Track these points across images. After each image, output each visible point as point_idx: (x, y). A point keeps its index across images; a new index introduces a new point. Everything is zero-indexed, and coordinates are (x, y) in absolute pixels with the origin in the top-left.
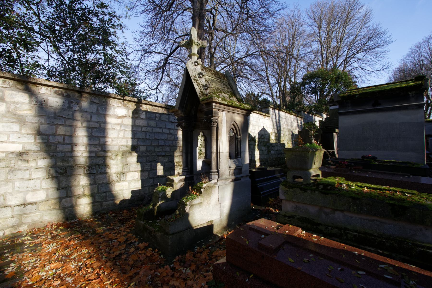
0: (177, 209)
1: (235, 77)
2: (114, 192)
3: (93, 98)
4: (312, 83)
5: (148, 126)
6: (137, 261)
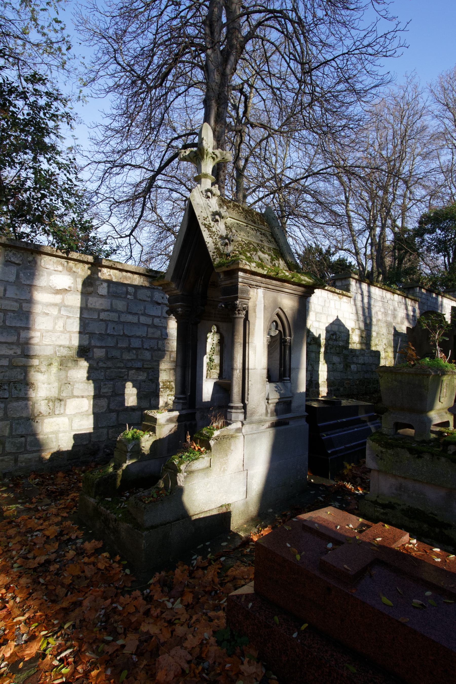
0: (160, 478)
1: (283, 217)
2: (41, 437)
3: (11, 254)
4: (439, 231)
5: (112, 310)
6: (78, 577)
